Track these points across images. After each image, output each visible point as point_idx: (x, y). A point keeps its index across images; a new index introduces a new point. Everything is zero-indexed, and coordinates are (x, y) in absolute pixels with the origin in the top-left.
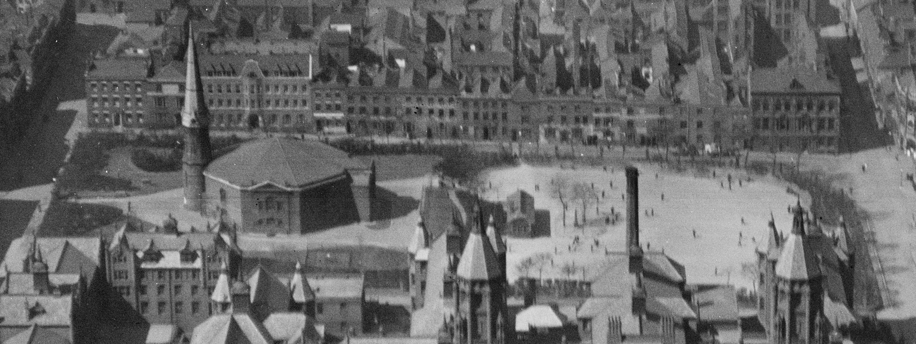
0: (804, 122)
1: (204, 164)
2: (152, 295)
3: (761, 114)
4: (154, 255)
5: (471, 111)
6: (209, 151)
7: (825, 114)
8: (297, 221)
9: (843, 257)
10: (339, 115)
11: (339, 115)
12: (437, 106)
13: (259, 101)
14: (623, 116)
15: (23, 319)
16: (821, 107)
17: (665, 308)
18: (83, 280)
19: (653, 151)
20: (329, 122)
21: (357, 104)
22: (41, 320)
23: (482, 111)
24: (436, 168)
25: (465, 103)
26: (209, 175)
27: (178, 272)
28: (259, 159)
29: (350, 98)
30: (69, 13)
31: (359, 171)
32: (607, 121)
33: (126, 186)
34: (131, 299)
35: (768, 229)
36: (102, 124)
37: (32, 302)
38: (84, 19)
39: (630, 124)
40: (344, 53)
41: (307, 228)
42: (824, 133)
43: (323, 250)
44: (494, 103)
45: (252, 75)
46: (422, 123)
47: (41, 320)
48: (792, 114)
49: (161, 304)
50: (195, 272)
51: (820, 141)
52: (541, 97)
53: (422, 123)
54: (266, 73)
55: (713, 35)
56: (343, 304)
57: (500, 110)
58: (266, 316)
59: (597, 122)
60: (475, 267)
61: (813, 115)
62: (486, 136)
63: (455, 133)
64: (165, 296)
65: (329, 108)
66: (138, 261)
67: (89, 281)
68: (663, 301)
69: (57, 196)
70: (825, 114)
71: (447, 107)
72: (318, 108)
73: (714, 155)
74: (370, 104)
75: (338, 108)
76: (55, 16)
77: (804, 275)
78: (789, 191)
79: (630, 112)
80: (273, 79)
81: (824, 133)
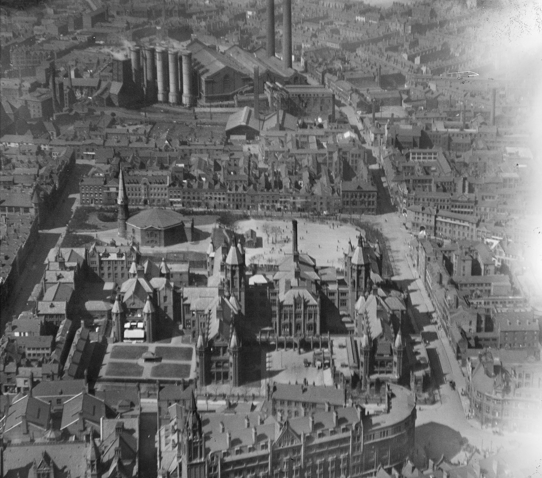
0: (362, 202)
3: (346, 199)
4: (107, 255)
6: (128, 214)
8: (163, 241)
9: (378, 256)
10: (179, 200)
11: (179, 200)
12: (218, 196)
13: (148, 194)
14: (291, 200)
15: (55, 280)
16: (369, 197)
17: (308, 276)
18: (78, 265)
20: (175, 203)
22: (62, 280)
23: (231, 198)
24: (218, 221)
25: (229, 195)
26: (128, 223)
27: (116, 261)
28: (147, 218)
29: (184, 193)
31: (187, 221)
32: (285, 202)
33: (95, 228)
34: (97, 272)
35: (348, 245)
37: (58, 274)
39: (294, 203)
40: (181, 175)
42: (370, 207)
43: (173, 253)
44: (241, 195)
46: (212, 203)
47: (62, 280)
48: (358, 199)
49: (109, 274)
51: (369, 210)
52: (259, 193)
55: (327, 168)
56: (181, 274)
57: (243, 198)
58: (151, 279)
59: (281, 202)
60: (233, 259)
61: (366, 200)
62: (237, 208)
63: (225, 207)
64: (111, 271)
65: (175, 197)
66: (100, 257)
68: (307, 273)
69: (68, 232)
72: (171, 197)
73: (327, 215)
75: (179, 197)
77: (363, 262)
78: (357, 229)
79: (294, 198)
80: (153, 185)
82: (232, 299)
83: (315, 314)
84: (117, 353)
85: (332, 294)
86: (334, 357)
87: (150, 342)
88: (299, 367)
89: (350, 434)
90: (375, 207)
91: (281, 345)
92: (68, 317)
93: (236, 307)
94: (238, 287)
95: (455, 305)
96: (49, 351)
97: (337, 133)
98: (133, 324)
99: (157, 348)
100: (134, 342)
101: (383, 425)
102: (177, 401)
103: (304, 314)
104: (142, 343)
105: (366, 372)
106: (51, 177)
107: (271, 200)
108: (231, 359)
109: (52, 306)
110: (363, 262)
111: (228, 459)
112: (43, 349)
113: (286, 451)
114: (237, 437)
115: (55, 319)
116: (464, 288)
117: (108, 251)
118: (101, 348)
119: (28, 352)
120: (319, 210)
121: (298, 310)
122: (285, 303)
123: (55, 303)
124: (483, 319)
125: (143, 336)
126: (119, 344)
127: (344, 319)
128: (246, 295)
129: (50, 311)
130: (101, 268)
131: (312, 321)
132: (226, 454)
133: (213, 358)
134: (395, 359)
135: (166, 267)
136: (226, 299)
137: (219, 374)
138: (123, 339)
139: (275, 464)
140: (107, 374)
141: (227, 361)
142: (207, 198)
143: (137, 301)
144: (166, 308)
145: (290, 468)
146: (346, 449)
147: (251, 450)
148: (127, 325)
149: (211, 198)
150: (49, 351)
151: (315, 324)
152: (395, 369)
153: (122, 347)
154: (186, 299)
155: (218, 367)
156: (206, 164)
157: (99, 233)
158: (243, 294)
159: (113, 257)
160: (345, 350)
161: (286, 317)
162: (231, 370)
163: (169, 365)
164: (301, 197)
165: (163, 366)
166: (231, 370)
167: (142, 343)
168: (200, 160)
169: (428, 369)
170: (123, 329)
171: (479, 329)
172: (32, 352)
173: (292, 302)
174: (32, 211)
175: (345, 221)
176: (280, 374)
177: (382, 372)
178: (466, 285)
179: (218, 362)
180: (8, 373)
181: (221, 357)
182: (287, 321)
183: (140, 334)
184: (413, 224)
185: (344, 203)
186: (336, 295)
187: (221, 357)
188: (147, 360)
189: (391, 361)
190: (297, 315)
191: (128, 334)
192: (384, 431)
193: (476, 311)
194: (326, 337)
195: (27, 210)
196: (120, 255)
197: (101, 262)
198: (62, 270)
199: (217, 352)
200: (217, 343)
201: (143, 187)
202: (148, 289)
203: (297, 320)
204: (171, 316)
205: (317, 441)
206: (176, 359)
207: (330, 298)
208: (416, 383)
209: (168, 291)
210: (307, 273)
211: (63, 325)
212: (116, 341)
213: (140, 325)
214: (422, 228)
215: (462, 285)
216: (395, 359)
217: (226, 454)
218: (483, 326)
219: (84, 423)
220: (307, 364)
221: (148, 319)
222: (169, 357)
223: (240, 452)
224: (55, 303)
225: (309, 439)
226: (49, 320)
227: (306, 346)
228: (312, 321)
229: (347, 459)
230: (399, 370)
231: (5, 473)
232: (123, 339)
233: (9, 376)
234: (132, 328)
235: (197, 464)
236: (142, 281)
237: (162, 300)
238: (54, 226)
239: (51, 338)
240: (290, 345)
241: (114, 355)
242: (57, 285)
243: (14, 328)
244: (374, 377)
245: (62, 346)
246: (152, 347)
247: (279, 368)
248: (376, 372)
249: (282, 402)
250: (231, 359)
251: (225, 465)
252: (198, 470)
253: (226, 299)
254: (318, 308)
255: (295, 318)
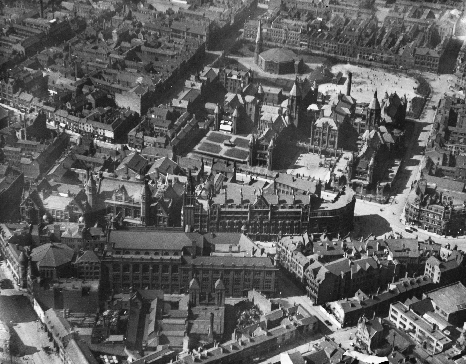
0: (429, 64)
1: (259, 53)
2: (229, 85)
3: (417, 60)
4: (231, 75)
5: (340, 48)
6: (261, 51)
7: (435, 63)
8: (278, 71)
9: (402, 104)
10: (306, 43)
11: (306, 43)
12: (331, 45)
13: (286, 36)
14: (380, 55)
15: (190, 87)
16: (434, 61)
17: (343, 111)
18: (208, 80)
19: (385, 65)
20: (303, 45)
21: (311, 41)
22: (194, 88)
23: (340, 48)
24: (322, 62)
25: (339, 45)
26: (260, 56)
27: (235, 80)
28: (272, 54)
29: (309, 39)
30: (254, 4)
31: (297, 60)
32: (376, 55)
33: (243, 55)
34: (224, 85)
35: (385, 94)
36: (247, 37)
37: (192, 83)
38: (260, 5)
39: (382, 57)
40: (318, 25)
41: (280, 73)
42: (434, 68)
43: (282, 79)
44: (347, 46)
45: (285, 30)
46: (327, 49)
47: (194, 88)
48: (426, 61)
49: (231, 88)
50: (240, 81)
51: (433, 70)
52: (359, 47)
53: (327, 49)
54: (289, 30)
55: (423, 34)
56: (274, 95)
57: (348, 49)
58: (245, 96)
59: (373, 55)
60: (294, 92)
61: (431, 62)
62: (343, 55)
63: (335, 53)
64: (232, 86)
65: (304, 41)
66: (226, 76)
67: (211, 81)
68: (343, 109)
69: (224, 55)
70: (435, 63)
71: (334, 45)
72: (301, 41)
73: (402, 69)
74: (314, 42)
75: (306, 42)
76: (248, 5)
77: (374, 108)
78: (416, 82)
79: (382, 54)
80: (290, 31)
81: (434, 68)
82: (287, 117)
83: (335, 136)
84: (212, 138)
85: (356, 124)
86: (337, 164)
87: (234, 134)
88: (316, 166)
89: (301, 210)
90: (437, 68)
91: (311, 151)
92: (188, 111)
93: (287, 121)
94: (294, 110)
95: (431, 145)
96: (167, 129)
97: (447, 9)
98: (226, 122)
99: (237, 139)
100: (225, 133)
101: (326, 209)
102: (222, 172)
103: (329, 135)
104: (229, 134)
105: (349, 177)
106: (230, 16)
107: (366, 52)
108: (268, 154)
109: (180, 102)
110: (374, 108)
111: (223, 209)
112: (163, 127)
113: (260, 212)
114: (231, 198)
115: (180, 111)
116: (455, 135)
117: (232, 73)
118: (203, 133)
119: (155, 127)
120: (398, 64)
121: (325, 131)
122: (317, 126)
123: (182, 101)
124: (448, 158)
125: (230, 130)
126: (217, 132)
127: (358, 142)
128: (299, 116)
129: (179, 105)
130: (227, 83)
131: (333, 139)
132: (223, 207)
133: (258, 151)
134: (369, 172)
135: (262, 89)
136: (282, 117)
137: (261, 161)
138: (219, 129)
139: (252, 218)
140: (199, 149)
141: (266, 154)
142: (324, 45)
143: (230, 108)
144: (250, 115)
145: (261, 222)
146: (298, 218)
147: (238, 207)
148: (222, 122)
149: (327, 46)
150: (167, 129)
151: (335, 142)
152: (368, 179)
153: (216, 134)
154: (263, 112)
155: (260, 157)
156: (339, 20)
157: (244, 59)
158: (297, 115)
159: (235, 77)
160: (347, 161)
161: (317, 135)
162: (268, 160)
163: (239, 150)
164: (388, 54)
165: (234, 150)
166: (268, 160)
167: (229, 134)
168: (337, 17)
169: (390, 183)
170: (220, 124)
171: (444, 164)
172: (157, 128)
173: (321, 126)
174: (205, 39)
175: (411, 75)
176: (302, 169)
177: (360, 179)
178: (456, 133)
179: (261, 154)
180: (138, 138)
181: (264, 152)
182: (317, 137)
183: (229, 128)
184: (456, 85)
185: (416, 62)
186: (358, 125)
187: (264, 152)
188: (226, 145)
189: (366, 173)
190: (324, 134)
191: (222, 127)
192: (324, 213)
193: (445, 152)
194: (340, 151)
195: (202, 37)
196: (239, 77)
197: (227, 79)
198: (196, 81)
199: (262, 148)
200: (263, 143)
201: (284, 31)
202: (241, 101)
203: (324, 137)
204: (253, 121)
205: (280, 210)
206: (244, 147)
207: (355, 127)
208: (379, 189)
209: (253, 106)
210: (343, 109)
211: (184, 115)
212: (215, 130)
213: (230, 123)
214: (461, 89)
215: (454, 133)
216: (369, 172)
217: (223, 207)
218: (448, 162)
219: (158, 174)
220: (321, 165)
221: (234, 120)
222: (241, 146)
223: (231, 207)
224: (182, 101)
225: (276, 208)
226: (177, 110)
227: (326, 153)
228: (333, 139)
229: (298, 224)
230: (370, 179)
231: (101, 192)
232: (219, 129)
233: (138, 140)
234: (225, 124)
235: (189, 208)
236: (239, 96)
237: (249, 110)
238: (215, 50)
239: (170, 122)
240: (316, 151)
241: (209, 139)
242: (189, 90)
243: (152, 112)
244: (353, 181)
245: (176, 128)
246: (234, 138)
247: (303, 165)
248: (356, 178)
249: (280, 184)
250: (268, 154)
251: (220, 212)
252: (189, 211)
253: (282, 117)
254: (337, 132)
255: (323, 136)
